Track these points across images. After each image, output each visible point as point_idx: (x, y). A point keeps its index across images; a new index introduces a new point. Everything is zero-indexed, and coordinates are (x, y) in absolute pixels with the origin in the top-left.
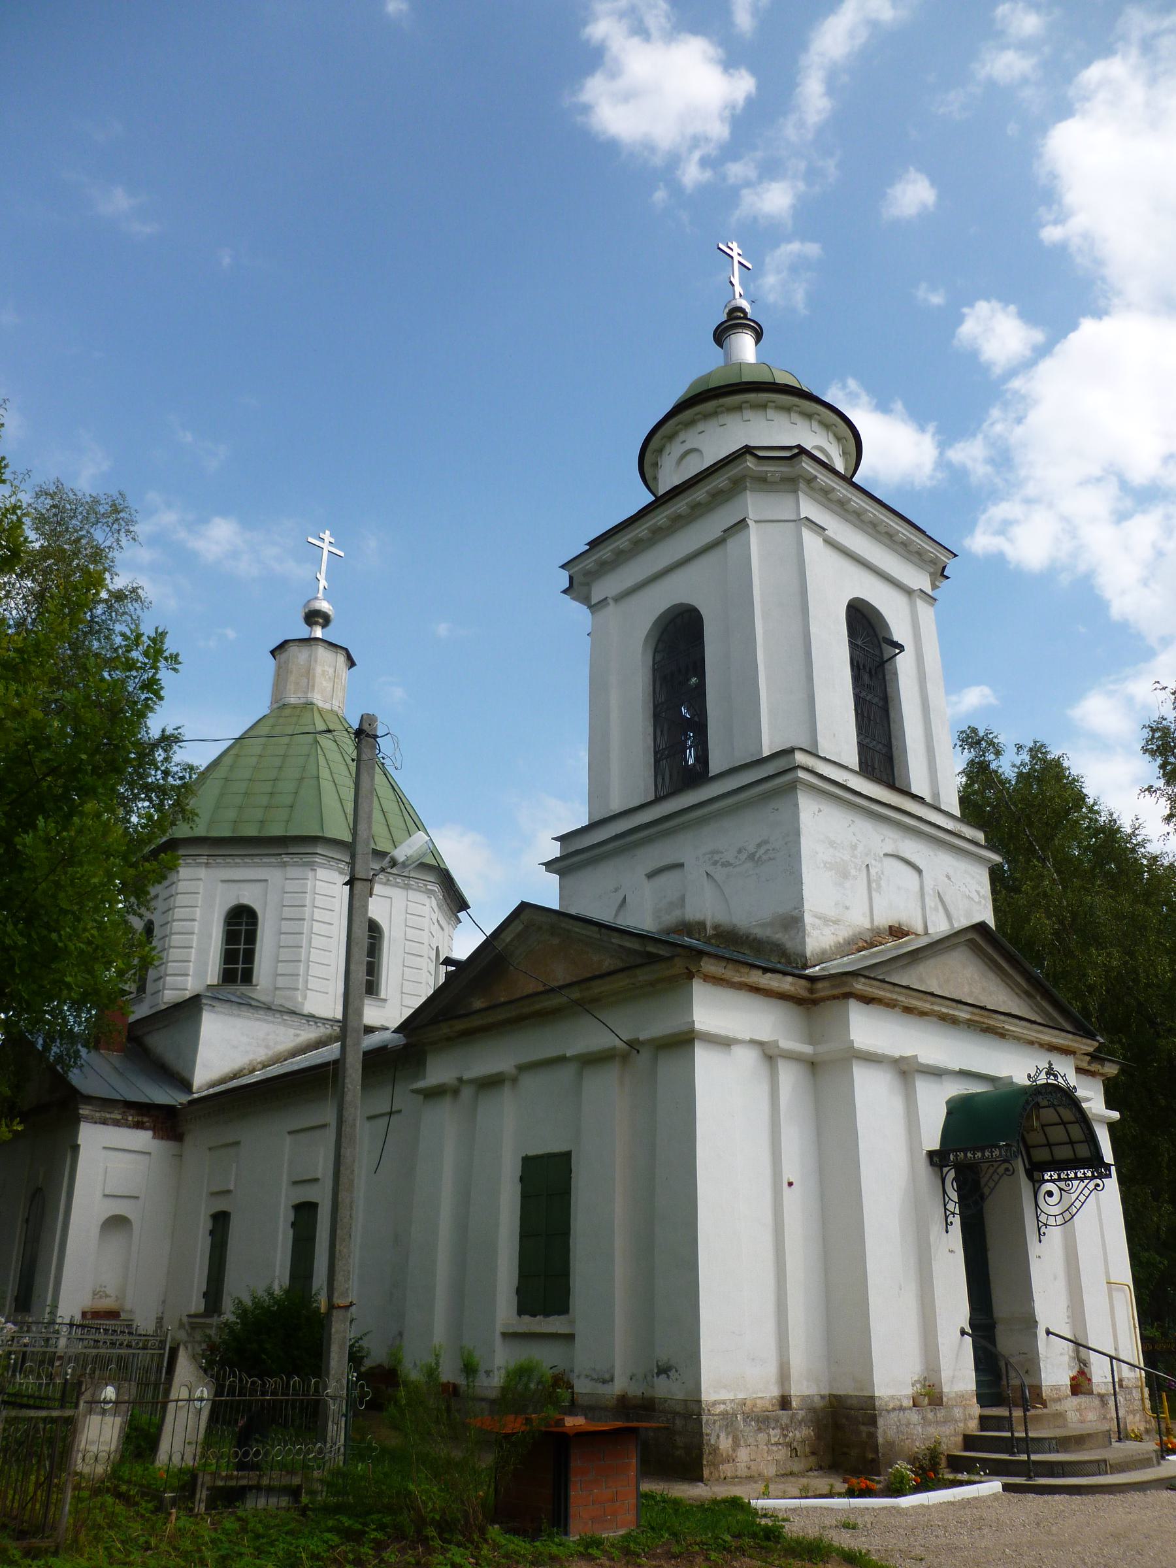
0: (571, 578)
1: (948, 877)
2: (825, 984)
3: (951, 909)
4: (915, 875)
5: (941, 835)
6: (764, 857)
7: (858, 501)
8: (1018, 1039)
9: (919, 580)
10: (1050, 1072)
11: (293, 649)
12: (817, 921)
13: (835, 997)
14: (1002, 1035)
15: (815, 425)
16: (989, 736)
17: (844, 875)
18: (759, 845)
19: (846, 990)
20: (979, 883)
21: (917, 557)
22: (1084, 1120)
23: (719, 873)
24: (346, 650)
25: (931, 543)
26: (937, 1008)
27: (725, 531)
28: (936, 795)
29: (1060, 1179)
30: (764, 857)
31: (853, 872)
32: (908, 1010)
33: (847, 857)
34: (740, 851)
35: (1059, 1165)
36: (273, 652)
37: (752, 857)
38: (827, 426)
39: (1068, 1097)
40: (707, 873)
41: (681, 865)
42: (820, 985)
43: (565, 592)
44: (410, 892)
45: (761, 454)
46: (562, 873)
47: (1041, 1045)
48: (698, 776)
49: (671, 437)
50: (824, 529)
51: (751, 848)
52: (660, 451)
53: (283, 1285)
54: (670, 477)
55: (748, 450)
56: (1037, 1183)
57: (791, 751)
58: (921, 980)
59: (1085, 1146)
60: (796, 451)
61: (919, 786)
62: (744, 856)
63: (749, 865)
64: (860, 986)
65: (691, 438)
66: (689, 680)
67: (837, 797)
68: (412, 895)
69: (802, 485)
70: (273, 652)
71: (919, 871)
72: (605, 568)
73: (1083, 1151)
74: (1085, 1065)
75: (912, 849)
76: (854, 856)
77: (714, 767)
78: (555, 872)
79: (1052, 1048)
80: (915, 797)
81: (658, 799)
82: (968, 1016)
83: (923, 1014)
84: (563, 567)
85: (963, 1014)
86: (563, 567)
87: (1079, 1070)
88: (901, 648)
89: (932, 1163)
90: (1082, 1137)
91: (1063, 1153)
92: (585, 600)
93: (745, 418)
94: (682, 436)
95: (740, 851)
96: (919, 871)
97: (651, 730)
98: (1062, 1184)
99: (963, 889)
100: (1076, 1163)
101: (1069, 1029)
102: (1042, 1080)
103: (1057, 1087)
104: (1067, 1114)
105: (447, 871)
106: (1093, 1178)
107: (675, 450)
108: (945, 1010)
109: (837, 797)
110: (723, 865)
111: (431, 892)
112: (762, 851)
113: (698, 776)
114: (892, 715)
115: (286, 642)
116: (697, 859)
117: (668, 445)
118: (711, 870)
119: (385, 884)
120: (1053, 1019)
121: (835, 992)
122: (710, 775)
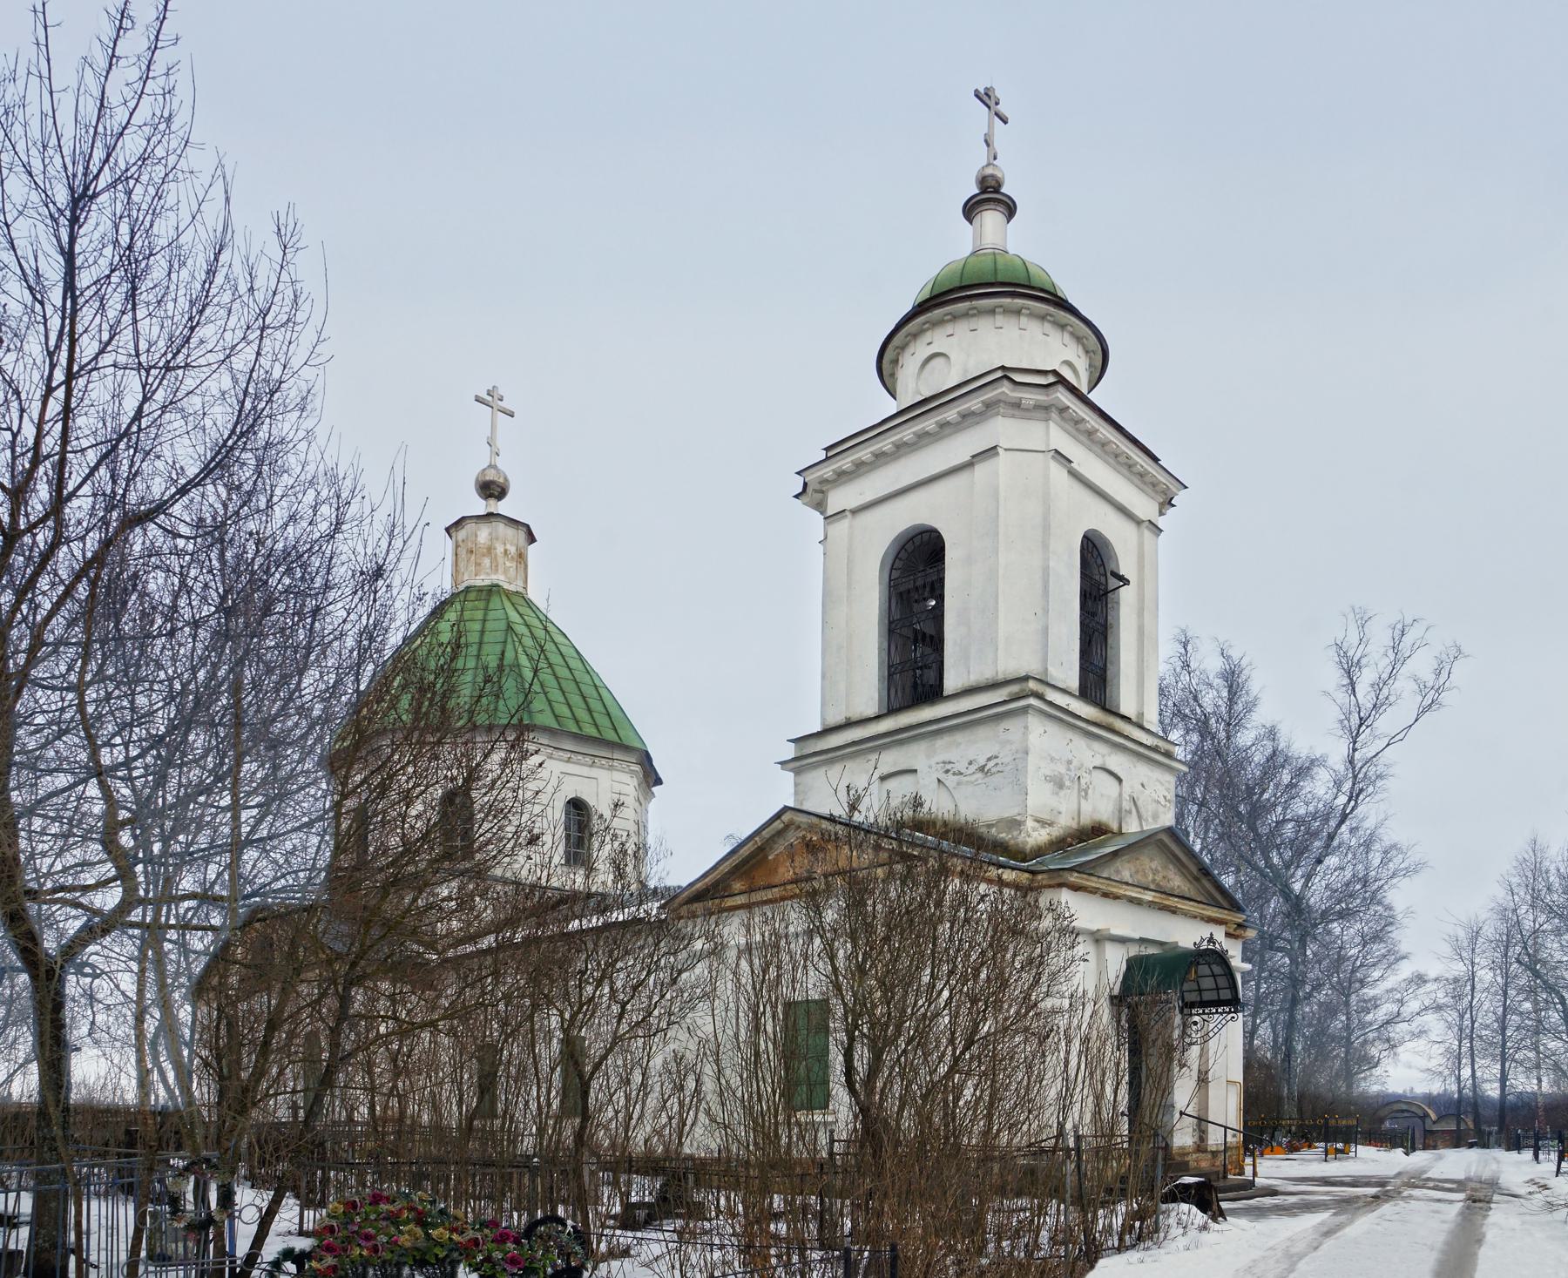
0: (805, 485)
1: (1143, 785)
2: (1045, 876)
3: (1142, 810)
4: (1114, 782)
5: (1141, 750)
6: (993, 770)
7: (1093, 421)
8: (1186, 914)
9: (1144, 506)
10: (1211, 940)
11: (469, 527)
12: (1036, 825)
13: (1050, 886)
14: (1174, 911)
15: (1067, 336)
16: (1544, 1039)
17: (1061, 786)
18: (989, 759)
19: (1061, 881)
20: (1168, 790)
21: (1142, 480)
22: (1229, 972)
23: (950, 780)
24: (528, 526)
25: (1167, 476)
26: (1128, 893)
27: (973, 457)
28: (1141, 715)
29: (1204, 1013)
30: (993, 770)
31: (1067, 783)
32: (1106, 895)
33: (1063, 770)
34: (970, 763)
35: (1204, 1004)
36: (447, 530)
37: (982, 769)
38: (1078, 339)
39: (1221, 958)
40: (939, 780)
41: (915, 771)
42: (1040, 877)
43: (797, 496)
44: (614, 773)
45: (1018, 378)
46: (798, 772)
47: (1202, 919)
48: (933, 693)
49: (915, 336)
50: (1071, 462)
51: (982, 762)
52: (903, 348)
53: (1433, 1064)
54: (914, 383)
55: (1006, 373)
56: (1186, 1016)
57: (1026, 678)
58: (1118, 872)
59: (1228, 991)
60: (1051, 379)
61: (1127, 706)
62: (973, 768)
63: (980, 775)
64: (1074, 878)
65: (938, 340)
66: (925, 599)
67: (1061, 720)
68: (617, 776)
69: (1054, 415)
70: (447, 530)
71: (1120, 780)
72: (842, 477)
73: (1226, 995)
74: (1231, 931)
75: (1117, 762)
76: (1069, 770)
77: (951, 683)
78: (791, 770)
79: (1210, 920)
80: (1124, 717)
81: (891, 711)
82: (1150, 899)
83: (1116, 897)
84: (799, 473)
85: (1148, 896)
86: (799, 473)
87: (1228, 935)
88: (1126, 582)
89: (1112, 1003)
90: (1227, 985)
91: (1207, 996)
92: (820, 506)
93: (998, 325)
94: (928, 337)
95: (970, 763)
96: (1120, 780)
97: (885, 645)
98: (1205, 1017)
99: (1153, 795)
100: (1218, 1003)
101: (1226, 906)
102: (1204, 946)
103: (1214, 952)
104: (1217, 969)
105: (647, 752)
106: (1230, 1012)
107: (920, 350)
108: (1134, 895)
109: (1061, 720)
110: (954, 774)
111: (632, 772)
112: (991, 764)
113: (933, 693)
114: (1110, 641)
115: (463, 519)
116: (930, 767)
117: (912, 345)
118: (943, 777)
119: (591, 766)
120: (1214, 898)
121: (1052, 883)
122: (945, 694)
